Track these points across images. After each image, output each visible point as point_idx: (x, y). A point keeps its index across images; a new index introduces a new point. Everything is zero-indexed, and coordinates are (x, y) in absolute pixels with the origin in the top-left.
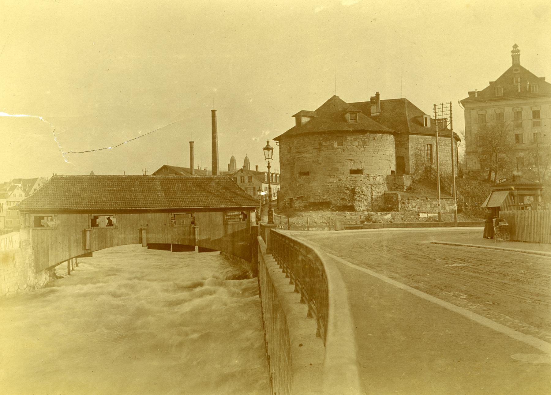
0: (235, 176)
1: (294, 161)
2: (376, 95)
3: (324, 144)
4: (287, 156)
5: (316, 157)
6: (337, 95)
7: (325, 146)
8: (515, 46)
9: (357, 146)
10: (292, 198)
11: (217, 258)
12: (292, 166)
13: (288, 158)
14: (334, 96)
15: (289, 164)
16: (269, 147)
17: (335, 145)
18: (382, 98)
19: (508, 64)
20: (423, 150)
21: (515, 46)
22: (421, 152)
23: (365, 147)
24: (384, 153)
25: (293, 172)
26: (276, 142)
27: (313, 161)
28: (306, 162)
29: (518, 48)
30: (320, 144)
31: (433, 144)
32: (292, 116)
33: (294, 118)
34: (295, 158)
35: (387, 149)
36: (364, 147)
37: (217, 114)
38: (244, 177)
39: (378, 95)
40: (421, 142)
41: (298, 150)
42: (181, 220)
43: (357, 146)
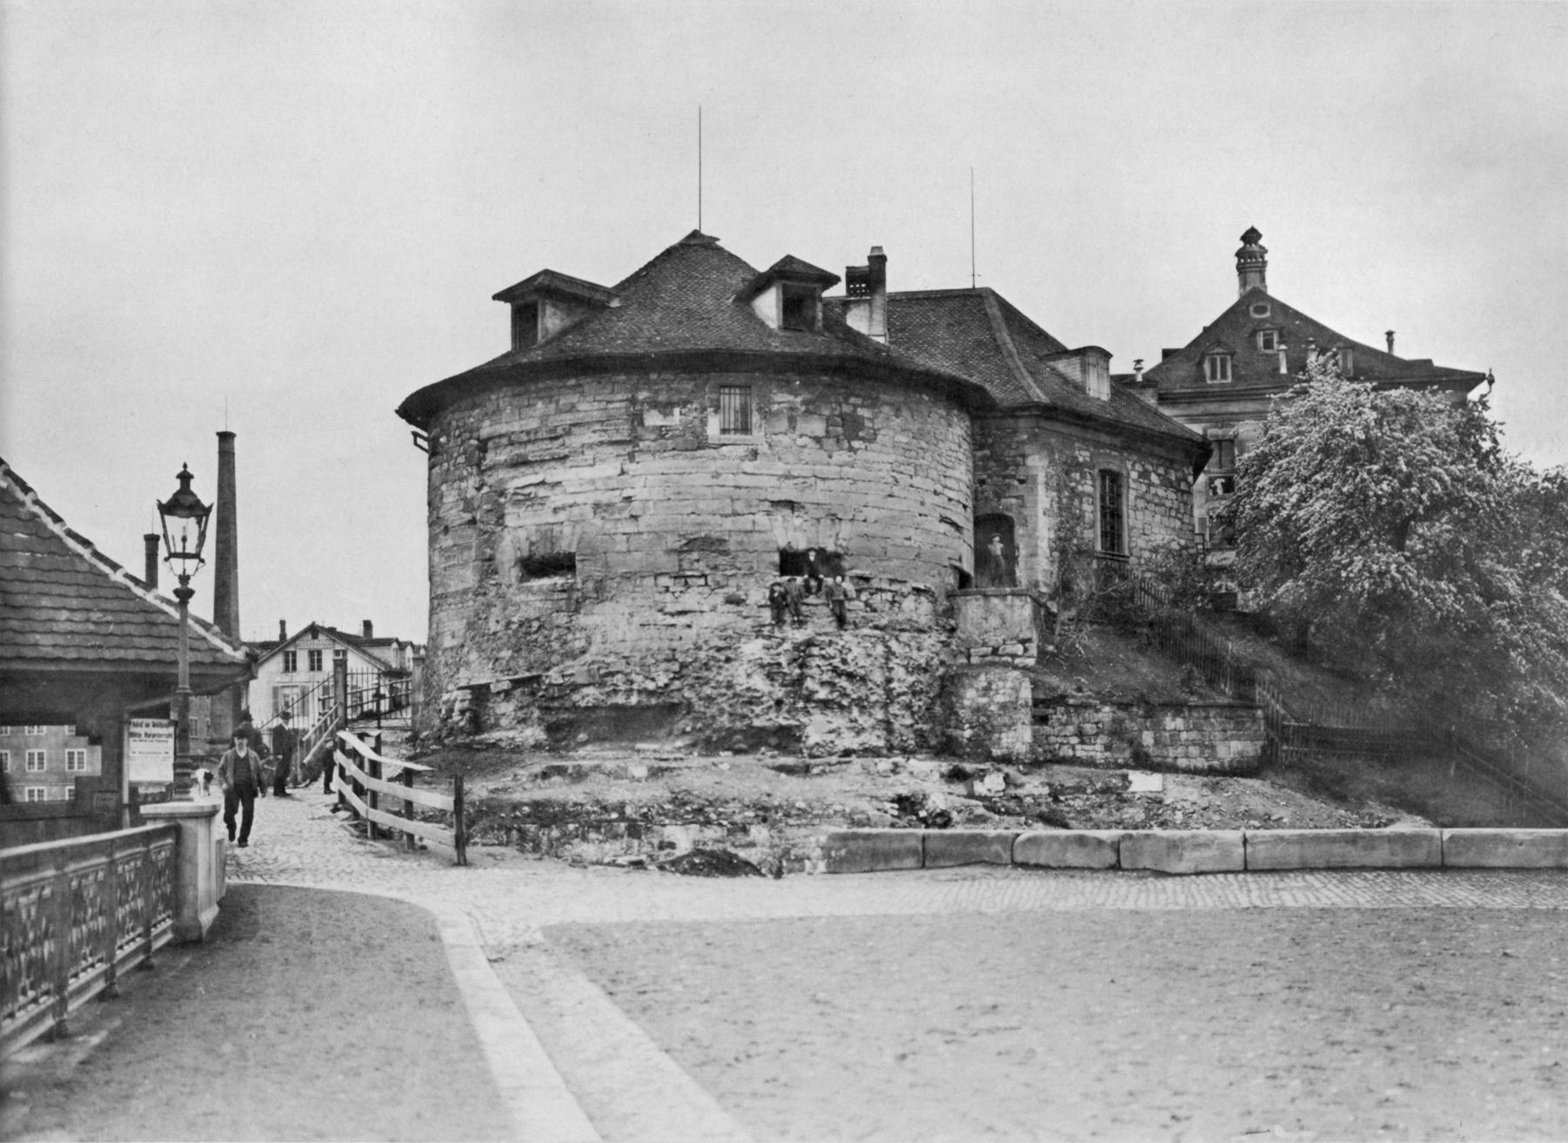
0: (291, 649)
1: (502, 506)
2: (870, 258)
3: (653, 419)
4: (464, 485)
5: (613, 484)
6: (703, 232)
7: (661, 432)
8: (1251, 236)
9: (817, 440)
10: (487, 686)
11: (1236, 436)
12: (488, 528)
13: (471, 493)
14: (695, 234)
15: (473, 522)
16: (188, 500)
17: (713, 427)
18: (897, 281)
19: (1225, 293)
20: (1089, 495)
21: (1251, 236)
22: (1081, 502)
23: (856, 444)
24: (939, 488)
25: (491, 559)
26: (416, 435)
27: (597, 506)
28: (563, 508)
29: (1262, 242)
30: (637, 419)
31: (1124, 472)
32: (497, 297)
33: (505, 309)
34: (502, 494)
35: (949, 473)
36: (851, 449)
37: (239, 446)
38: (319, 653)
39: (878, 260)
40: (1081, 459)
41: (522, 451)
42: (27, 789)
43: (817, 440)
